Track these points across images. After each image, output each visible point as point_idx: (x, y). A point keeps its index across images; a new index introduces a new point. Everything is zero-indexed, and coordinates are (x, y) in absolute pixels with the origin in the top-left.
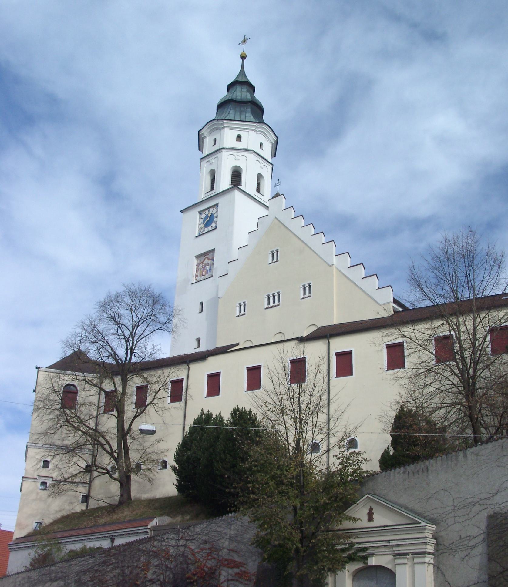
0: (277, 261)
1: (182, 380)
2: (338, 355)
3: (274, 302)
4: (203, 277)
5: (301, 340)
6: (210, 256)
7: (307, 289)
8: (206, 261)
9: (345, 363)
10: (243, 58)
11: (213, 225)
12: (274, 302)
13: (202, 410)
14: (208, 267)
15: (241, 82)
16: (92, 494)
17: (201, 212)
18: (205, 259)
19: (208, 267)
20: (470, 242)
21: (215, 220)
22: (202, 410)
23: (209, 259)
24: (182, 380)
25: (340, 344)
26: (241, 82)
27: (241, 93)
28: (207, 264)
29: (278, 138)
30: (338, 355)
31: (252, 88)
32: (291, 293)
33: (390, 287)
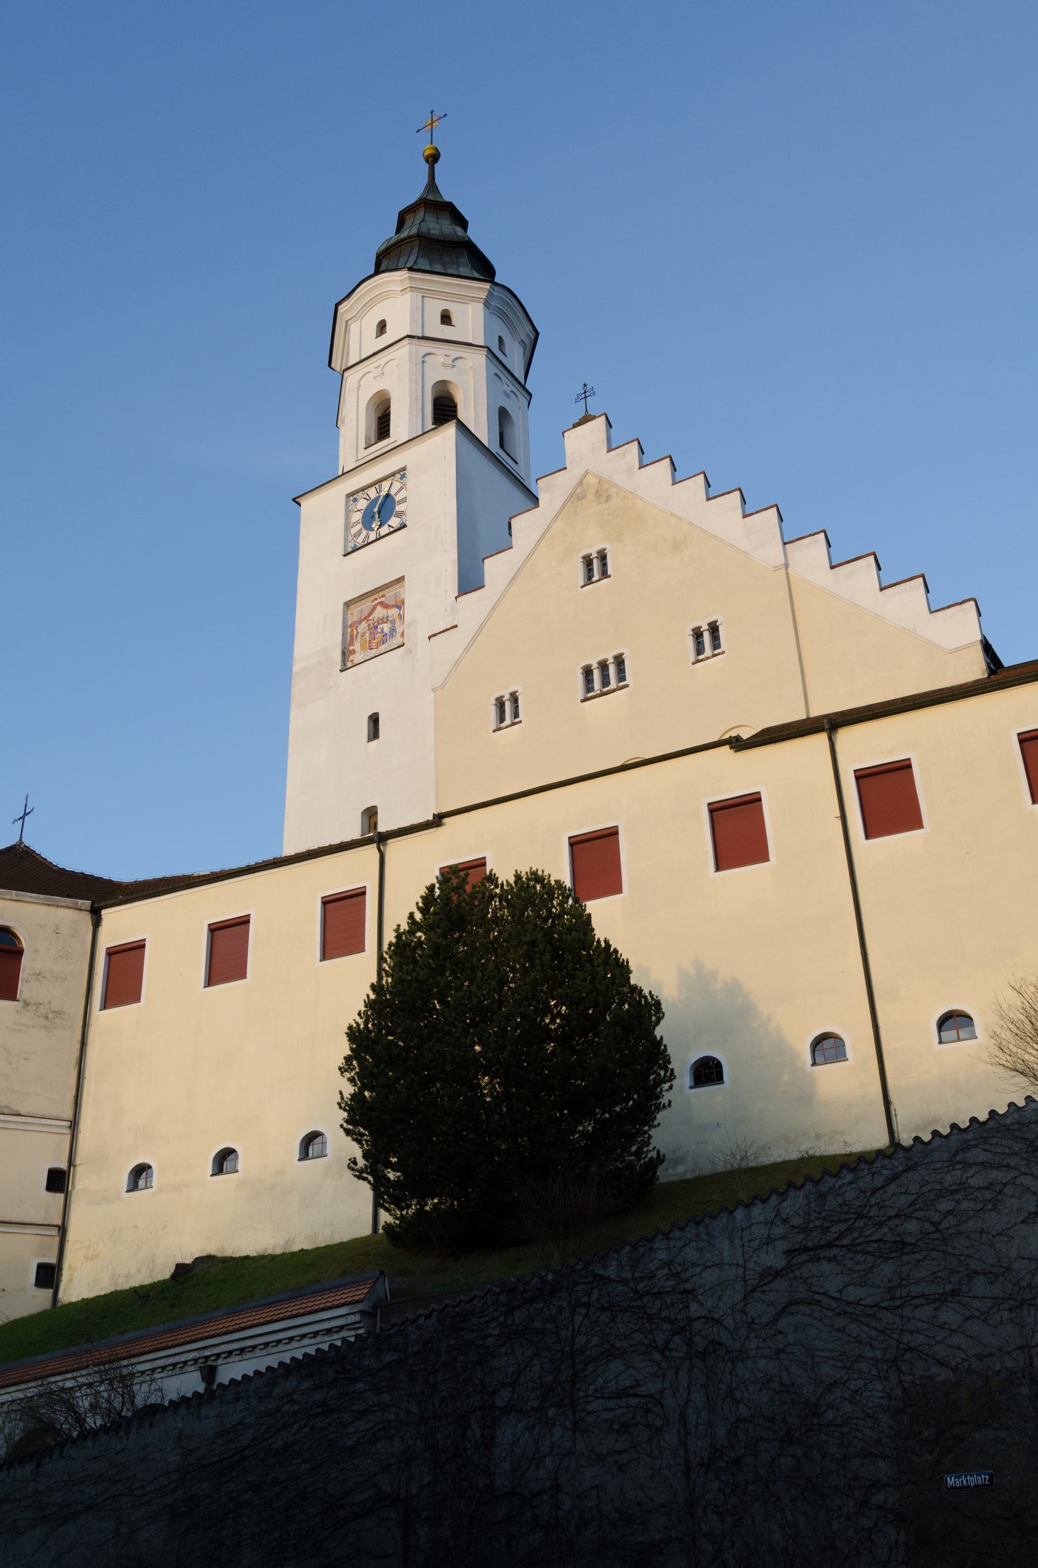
0: (605, 574)
1: (360, 894)
2: (861, 776)
3: (605, 682)
4: (374, 652)
5: (737, 744)
6: (389, 595)
7: (707, 637)
8: (380, 612)
9: (888, 799)
10: (433, 158)
11: (394, 522)
12: (605, 682)
13: (341, 1093)
14: (386, 628)
15: (432, 203)
16: (393, 847)
17: (352, 496)
18: (374, 608)
19: (386, 628)
20: (366, 1362)
21: (398, 508)
22: (341, 1093)
23: (386, 606)
24: (360, 894)
25: (867, 746)
26: (432, 203)
27: (440, 227)
28: (384, 620)
29: (537, 334)
30: (861, 776)
31: (464, 223)
32: (658, 658)
33: (972, 603)
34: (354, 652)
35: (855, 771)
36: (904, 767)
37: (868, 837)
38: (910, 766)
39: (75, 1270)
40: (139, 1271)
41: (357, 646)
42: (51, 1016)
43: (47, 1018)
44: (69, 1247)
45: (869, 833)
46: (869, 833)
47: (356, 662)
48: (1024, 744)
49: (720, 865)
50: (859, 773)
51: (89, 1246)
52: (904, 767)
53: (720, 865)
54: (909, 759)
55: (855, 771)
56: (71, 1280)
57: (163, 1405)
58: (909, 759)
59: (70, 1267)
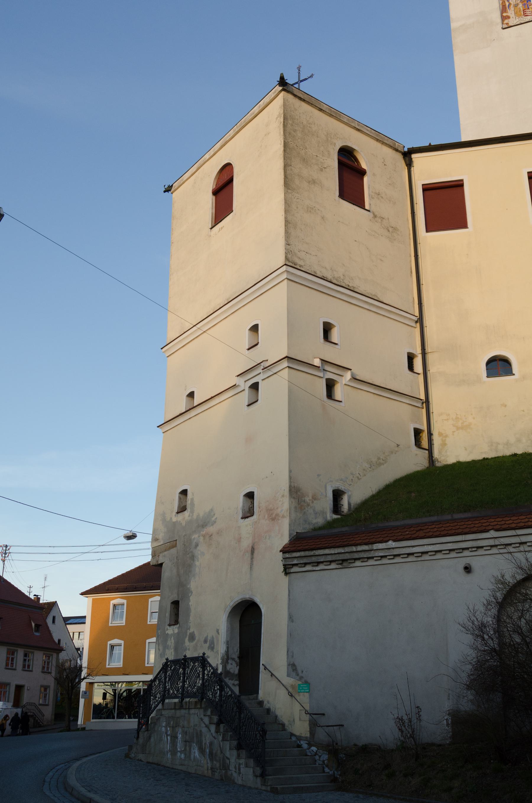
2: (427, 189)
30: (427, 189)
34: (508, 17)
35: (423, 185)
36: (459, 185)
37: (428, 231)
38: (462, 185)
39: (446, 436)
40: (519, 441)
41: (511, 13)
42: (391, 229)
43: (389, 231)
44: (434, 418)
45: (428, 229)
46: (428, 229)
47: (511, 24)
48: (428, 193)
49: (463, 224)
50: (425, 187)
51: (457, 418)
52: (459, 185)
53: (463, 224)
54: (462, 180)
55: (423, 185)
56: (444, 444)
57: (160, 601)
58: (462, 180)
59: (440, 434)
